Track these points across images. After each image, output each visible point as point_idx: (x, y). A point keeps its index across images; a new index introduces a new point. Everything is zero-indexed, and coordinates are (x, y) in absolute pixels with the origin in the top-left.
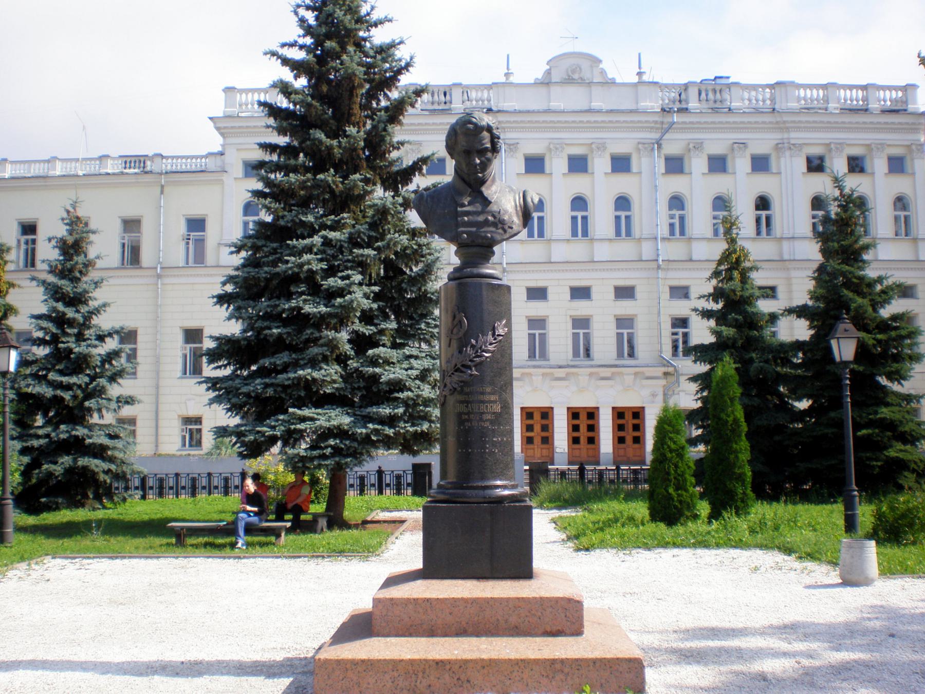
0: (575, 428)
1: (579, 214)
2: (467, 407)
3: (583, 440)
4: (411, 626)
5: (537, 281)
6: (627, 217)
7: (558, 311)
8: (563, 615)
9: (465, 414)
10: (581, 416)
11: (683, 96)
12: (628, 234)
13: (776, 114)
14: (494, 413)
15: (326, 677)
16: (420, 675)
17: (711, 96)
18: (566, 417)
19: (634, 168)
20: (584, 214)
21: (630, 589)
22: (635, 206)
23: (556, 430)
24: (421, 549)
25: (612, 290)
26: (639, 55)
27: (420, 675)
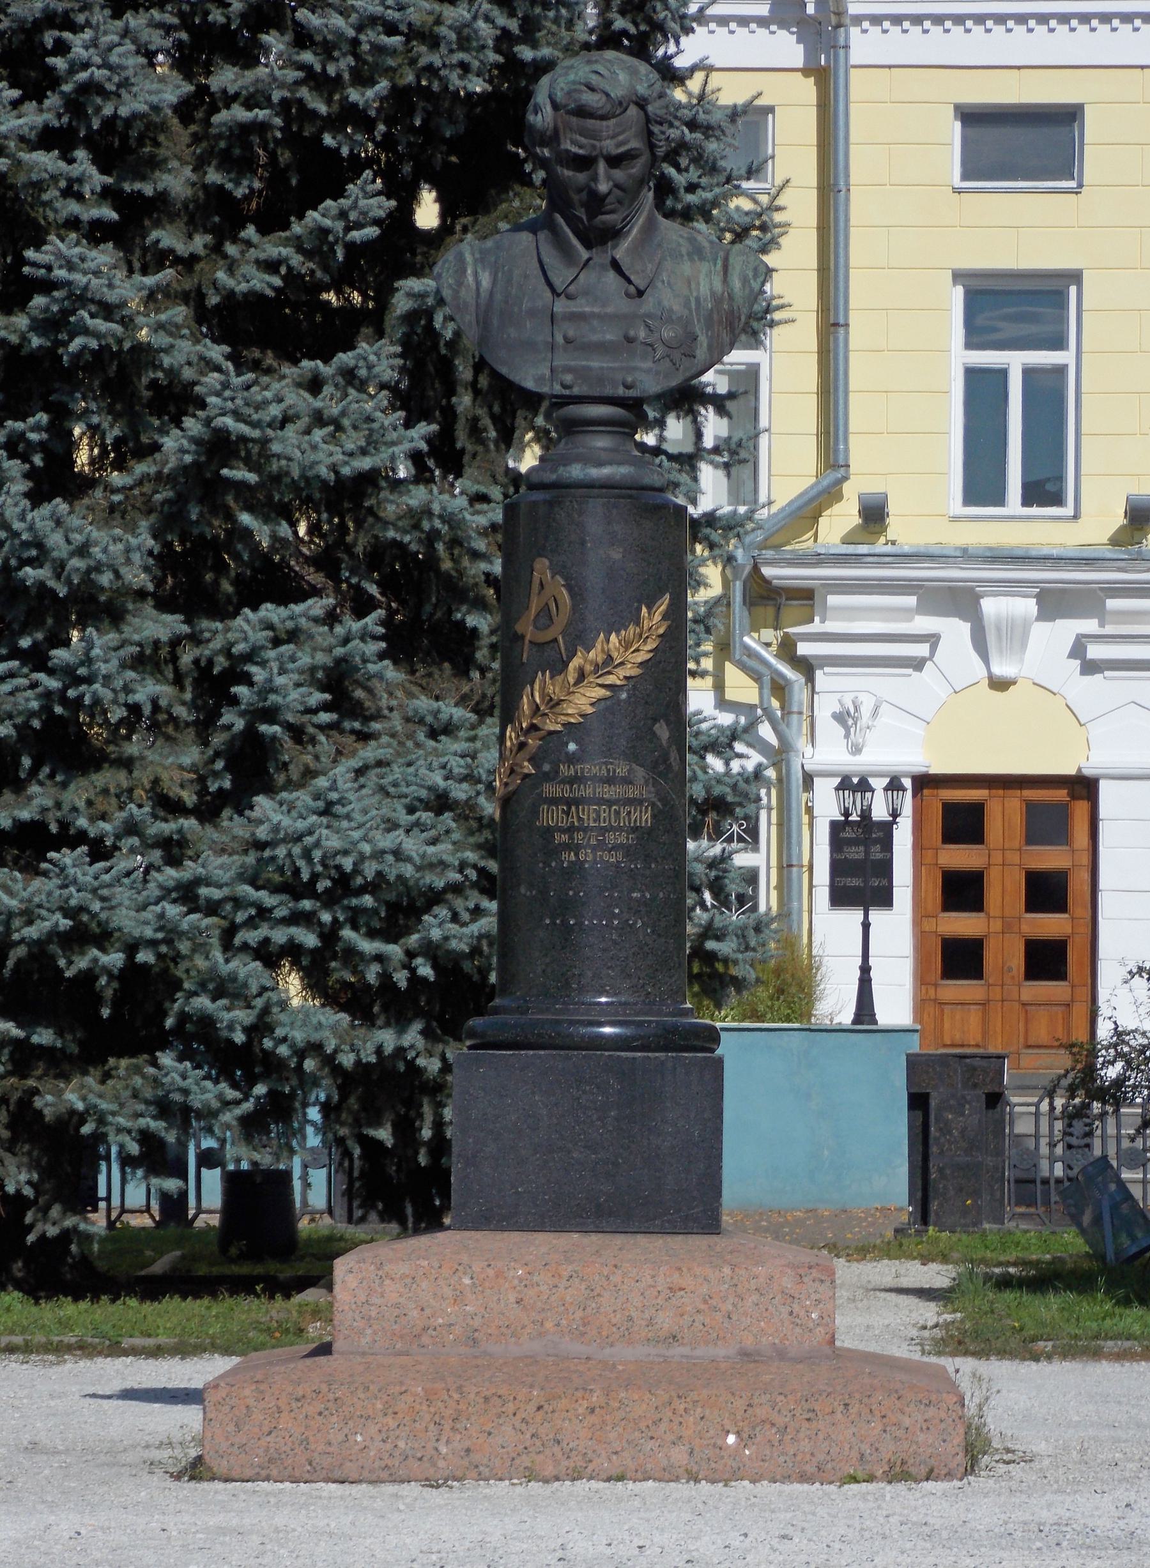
0: (1046, 892)
2: (567, 813)
8: (785, 1310)
9: (563, 831)
14: (635, 829)
15: (231, 1428)
27: (447, 1425)
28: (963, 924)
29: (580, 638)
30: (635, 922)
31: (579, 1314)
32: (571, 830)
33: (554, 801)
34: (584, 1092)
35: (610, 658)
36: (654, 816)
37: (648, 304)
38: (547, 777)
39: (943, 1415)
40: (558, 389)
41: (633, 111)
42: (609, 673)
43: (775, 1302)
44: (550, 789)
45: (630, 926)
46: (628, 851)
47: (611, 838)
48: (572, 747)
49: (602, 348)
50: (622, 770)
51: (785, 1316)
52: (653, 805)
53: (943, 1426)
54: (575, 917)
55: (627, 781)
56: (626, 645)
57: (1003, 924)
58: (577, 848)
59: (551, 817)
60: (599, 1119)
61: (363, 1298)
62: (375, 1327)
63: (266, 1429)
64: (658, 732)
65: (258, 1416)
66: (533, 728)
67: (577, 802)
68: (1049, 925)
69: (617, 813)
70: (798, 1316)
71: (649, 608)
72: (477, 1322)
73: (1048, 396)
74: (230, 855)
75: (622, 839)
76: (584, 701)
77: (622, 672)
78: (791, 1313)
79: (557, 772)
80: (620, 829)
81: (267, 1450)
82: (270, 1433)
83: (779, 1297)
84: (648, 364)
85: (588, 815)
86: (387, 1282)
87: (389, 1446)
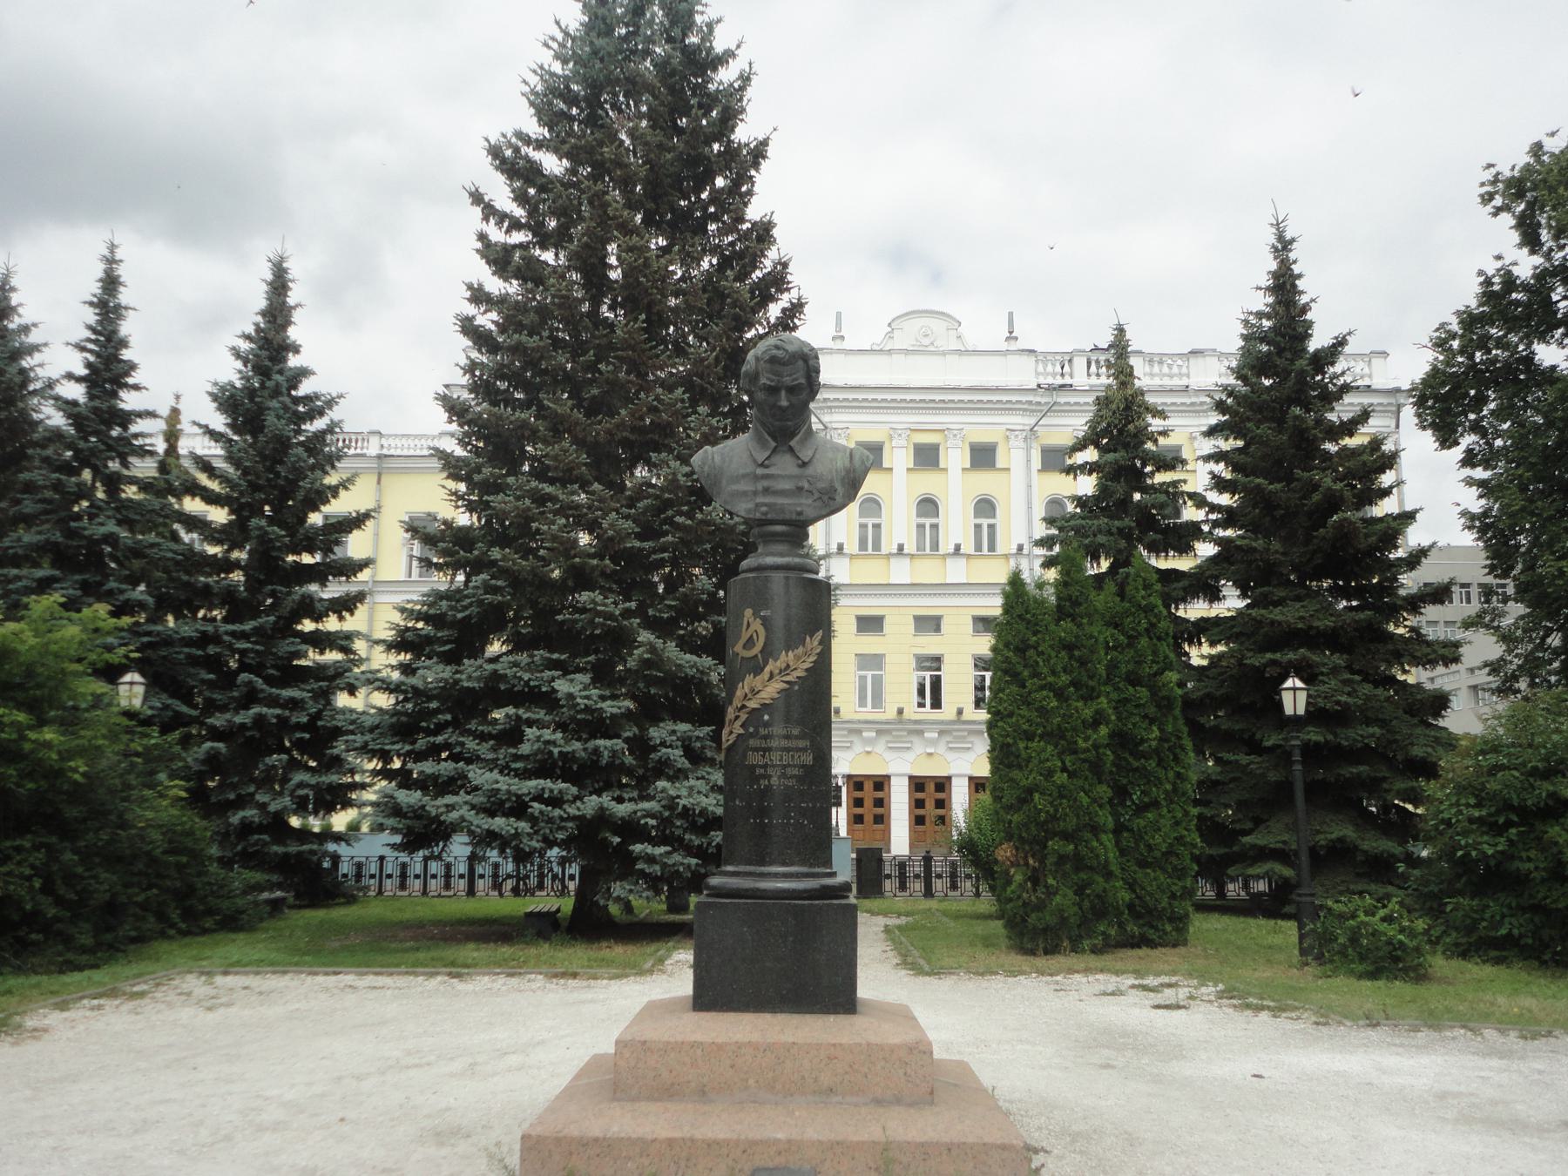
0: (880, 803)
1: (985, 522)
3: (869, 818)
5: (927, 605)
7: (900, 647)
8: (901, 1072)
10: (927, 804)
11: (1067, 368)
12: (992, 548)
14: (803, 766)
16: (683, 1164)
18: (906, 789)
19: (1001, 462)
20: (934, 521)
21: (1002, 1030)
23: (893, 807)
25: (854, 621)
27: (683, 1164)
28: (859, 811)
29: (768, 652)
31: (771, 1074)
32: (765, 766)
33: (756, 750)
35: (788, 666)
37: (809, 471)
38: (752, 735)
40: (758, 515)
41: (800, 363)
44: (752, 742)
46: (799, 778)
47: (790, 771)
48: (766, 717)
49: (782, 493)
56: (797, 658)
57: (930, 810)
58: (769, 777)
59: (754, 759)
66: (744, 706)
67: (769, 749)
68: (879, 811)
72: (705, 1080)
73: (878, 681)
75: (795, 772)
76: (771, 691)
84: (810, 501)
85: (775, 757)
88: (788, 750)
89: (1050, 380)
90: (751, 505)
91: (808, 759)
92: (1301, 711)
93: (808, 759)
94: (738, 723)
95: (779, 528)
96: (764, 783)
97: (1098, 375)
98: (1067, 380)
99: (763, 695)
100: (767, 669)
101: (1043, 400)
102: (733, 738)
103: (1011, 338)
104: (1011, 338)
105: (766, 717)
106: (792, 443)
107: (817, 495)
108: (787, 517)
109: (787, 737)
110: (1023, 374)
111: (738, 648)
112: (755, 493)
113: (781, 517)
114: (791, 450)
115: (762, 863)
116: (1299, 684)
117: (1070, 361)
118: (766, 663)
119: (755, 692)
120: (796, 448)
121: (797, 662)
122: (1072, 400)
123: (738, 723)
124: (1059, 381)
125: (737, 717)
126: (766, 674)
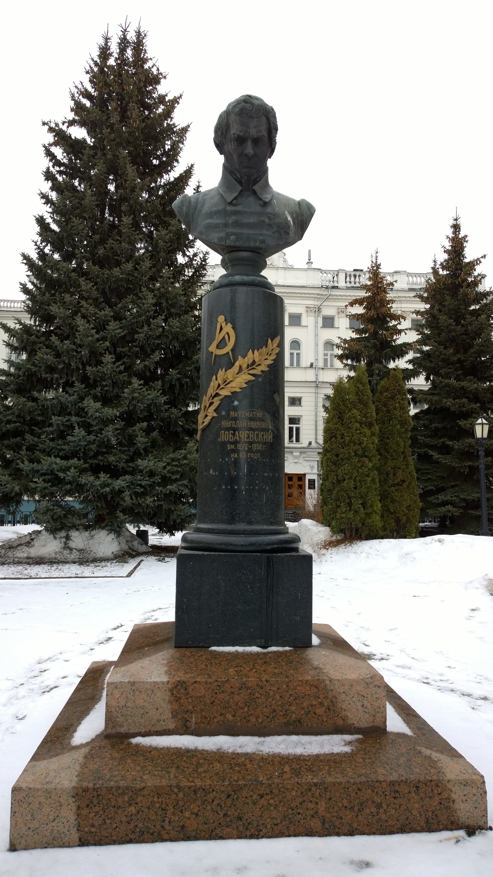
2: (234, 435)
4: (159, 721)
6: (298, 354)
8: (359, 704)
9: (232, 443)
10: (294, 479)
11: (335, 278)
12: (298, 364)
13: (394, 292)
14: (265, 443)
15: (29, 817)
17: (352, 279)
22: (303, 347)
24: (313, 573)
26: (310, 251)
30: (266, 488)
34: (243, 574)
36: (273, 437)
39: (474, 791)
41: (264, 118)
42: (254, 369)
43: (354, 699)
45: (264, 489)
47: (255, 446)
48: (236, 403)
50: (260, 414)
51: (360, 708)
52: (273, 432)
53: (475, 798)
54: (237, 485)
55: (262, 420)
59: (225, 436)
60: (251, 588)
61: (123, 704)
62: (130, 721)
63: (51, 818)
64: (275, 398)
65: (46, 809)
66: (217, 395)
69: (258, 435)
70: (366, 708)
71: (272, 341)
74: (454, 507)
75: (260, 447)
77: (260, 368)
78: (363, 706)
79: (229, 415)
80: (259, 443)
81: (52, 831)
82: (54, 820)
83: (356, 696)
84: (270, 233)
86: (137, 693)
87: (132, 826)
88: (250, 429)
89: (327, 284)
90: (222, 234)
91: (269, 437)
92: (485, 435)
93: (269, 437)
94: (213, 407)
95: (245, 254)
96: (234, 456)
97: (350, 282)
98: (336, 284)
99: (233, 384)
100: (237, 364)
101: (324, 293)
102: (207, 421)
103: (309, 262)
104: (309, 262)
105: (236, 403)
106: (256, 187)
107: (275, 228)
108: (252, 244)
109: (251, 419)
110: (316, 279)
111: (213, 348)
112: (226, 225)
113: (246, 245)
114: (254, 193)
115: (232, 521)
116: (485, 421)
117: (337, 275)
118: (235, 360)
119: (226, 382)
120: (258, 192)
121: (262, 358)
122: (338, 294)
123: (213, 407)
124: (332, 284)
125: (211, 404)
126: (236, 368)
